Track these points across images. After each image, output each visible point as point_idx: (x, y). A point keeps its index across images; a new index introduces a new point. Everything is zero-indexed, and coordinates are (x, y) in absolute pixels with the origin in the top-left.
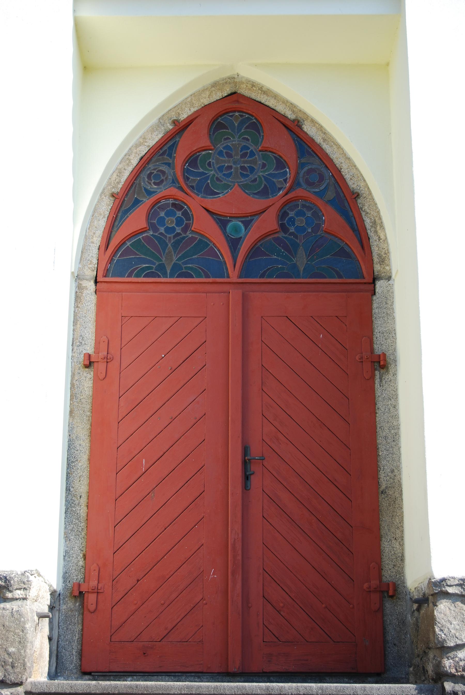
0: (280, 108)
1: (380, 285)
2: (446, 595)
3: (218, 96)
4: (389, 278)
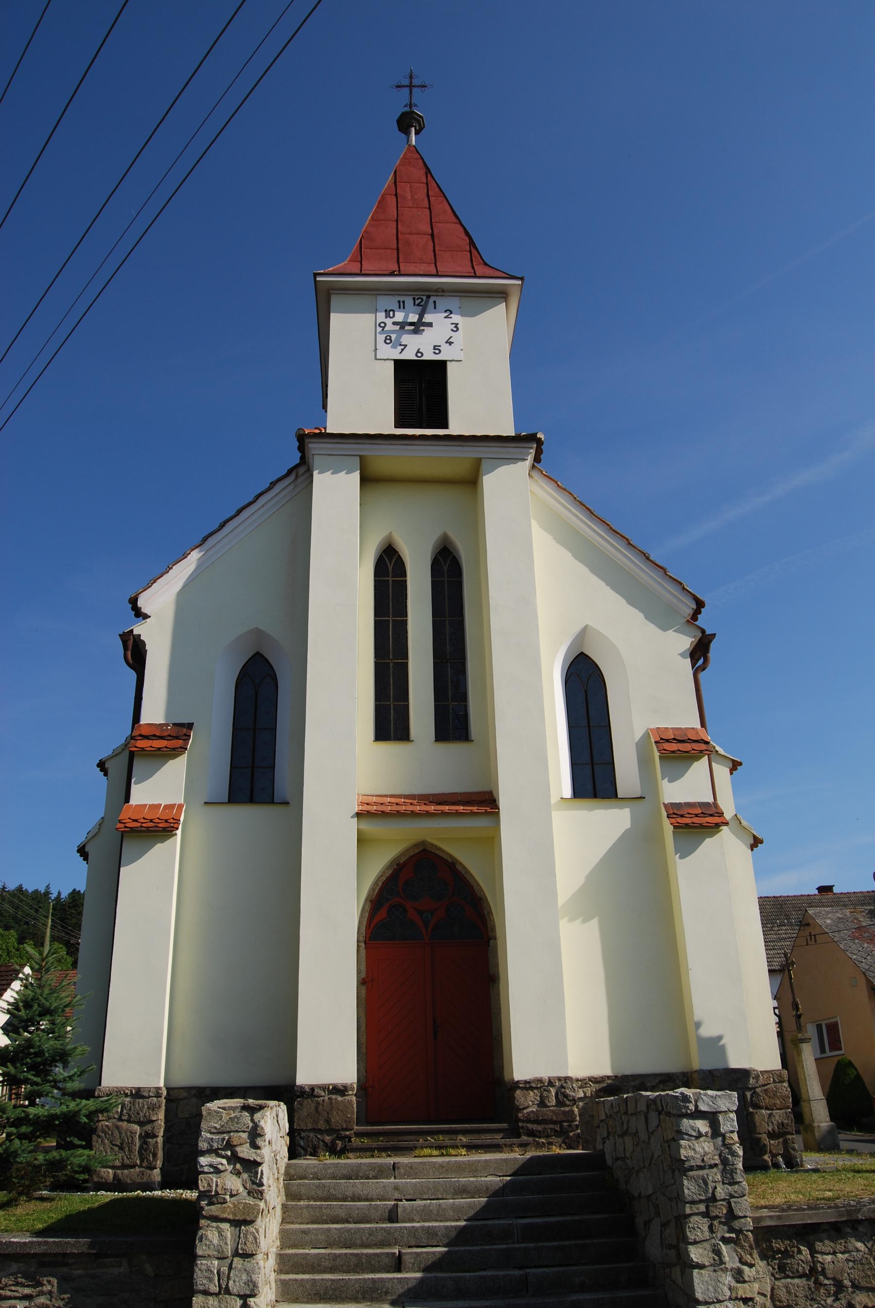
0: (445, 857)
1: (491, 942)
2: (520, 1088)
3: (417, 851)
4: (495, 939)
